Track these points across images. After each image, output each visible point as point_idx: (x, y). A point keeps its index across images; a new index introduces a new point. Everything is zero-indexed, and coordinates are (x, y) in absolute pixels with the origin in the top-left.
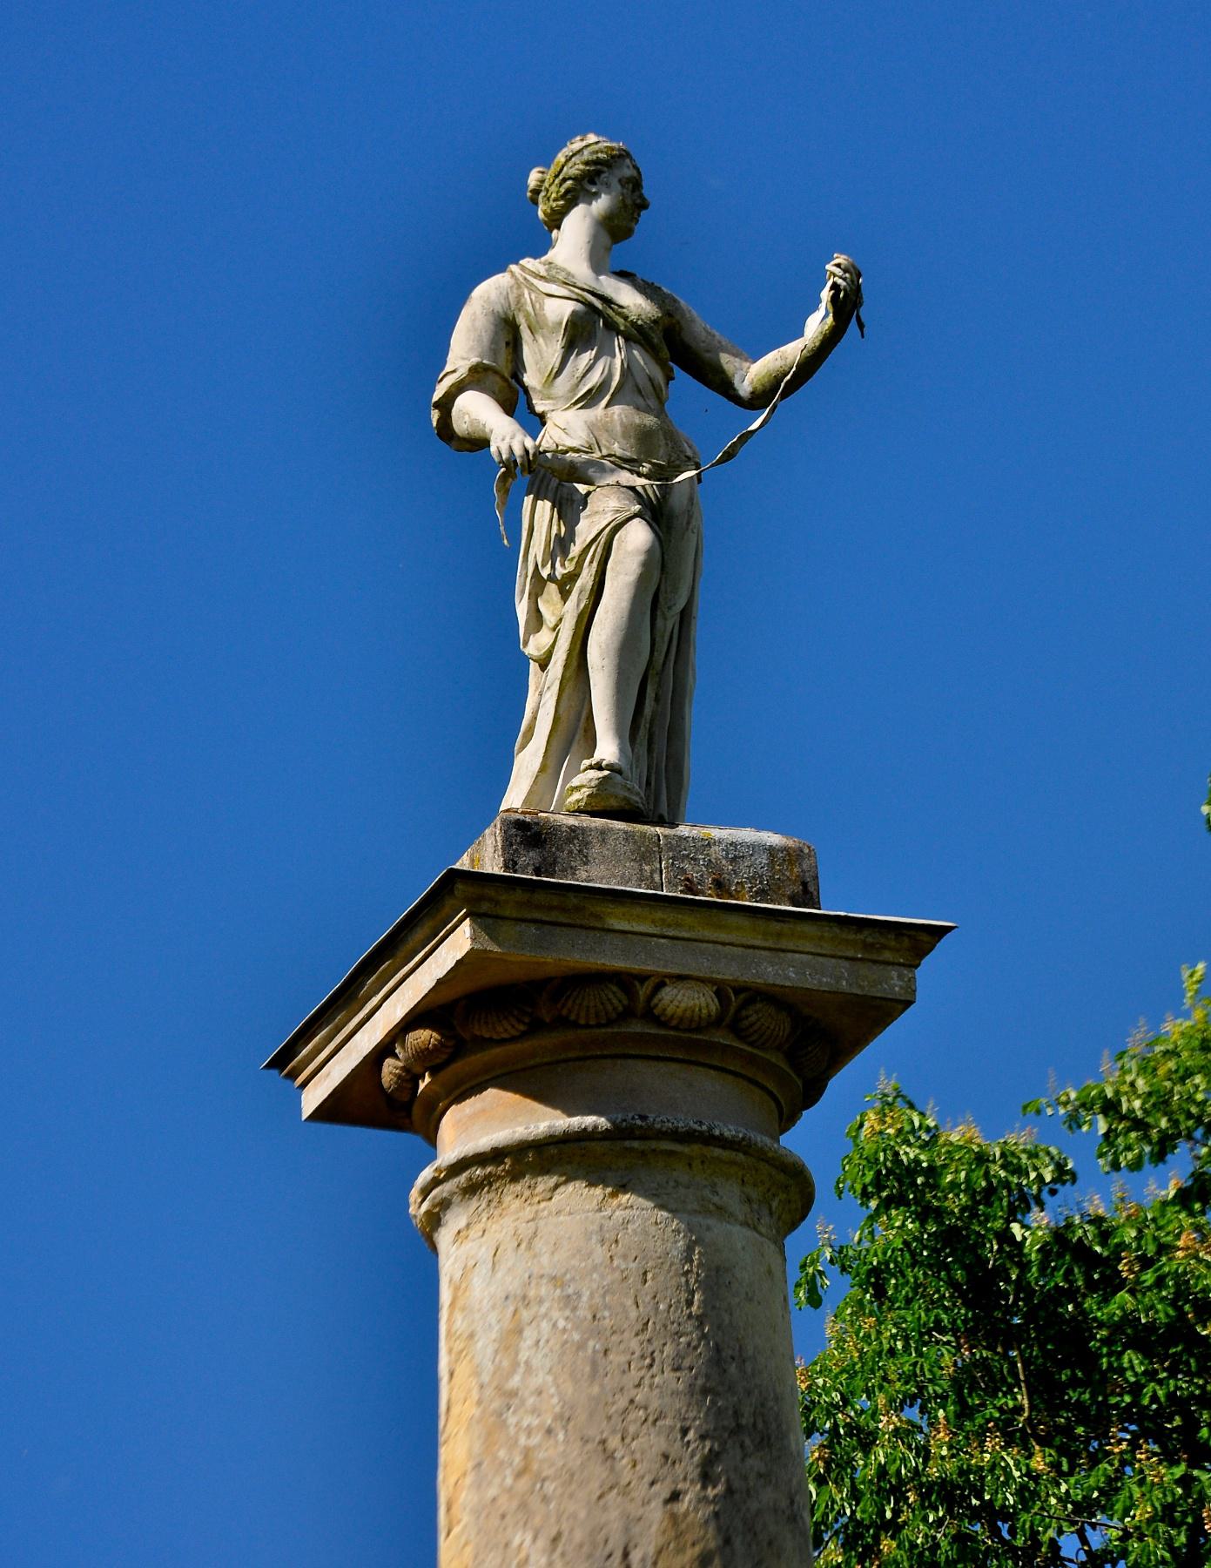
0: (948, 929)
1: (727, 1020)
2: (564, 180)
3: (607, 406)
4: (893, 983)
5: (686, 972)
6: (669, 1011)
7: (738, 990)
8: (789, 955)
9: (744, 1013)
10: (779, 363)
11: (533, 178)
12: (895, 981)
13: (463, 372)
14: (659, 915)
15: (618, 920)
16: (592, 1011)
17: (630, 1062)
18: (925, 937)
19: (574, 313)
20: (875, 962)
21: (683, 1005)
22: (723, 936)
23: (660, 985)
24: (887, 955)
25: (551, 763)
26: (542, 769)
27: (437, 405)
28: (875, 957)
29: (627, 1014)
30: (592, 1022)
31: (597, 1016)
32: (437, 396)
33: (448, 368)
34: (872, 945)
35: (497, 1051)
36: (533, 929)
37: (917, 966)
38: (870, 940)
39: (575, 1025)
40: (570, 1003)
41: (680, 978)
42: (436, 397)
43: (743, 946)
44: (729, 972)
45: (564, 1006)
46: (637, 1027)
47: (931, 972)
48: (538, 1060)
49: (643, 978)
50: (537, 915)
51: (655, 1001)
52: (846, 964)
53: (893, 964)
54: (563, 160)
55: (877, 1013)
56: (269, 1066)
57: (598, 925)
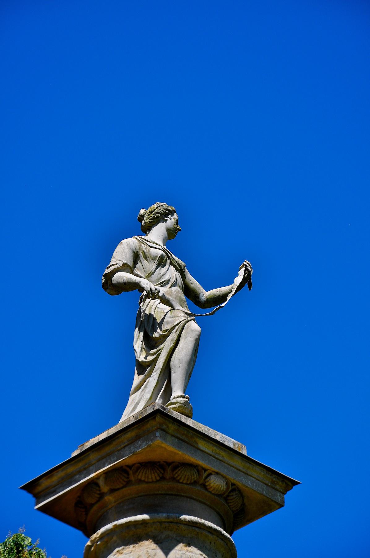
0: (298, 483)
1: (225, 495)
2: (157, 213)
3: (170, 287)
4: (278, 497)
5: (220, 472)
6: (209, 485)
7: (233, 484)
8: (251, 478)
9: (232, 494)
10: (218, 293)
11: (142, 211)
12: (279, 497)
13: (120, 264)
14: (215, 448)
15: (202, 445)
16: (187, 477)
17: (192, 501)
18: (290, 483)
19: (162, 255)
20: (273, 488)
21: (217, 484)
22: (231, 463)
23: (210, 474)
24: (277, 487)
25: (153, 397)
26: (151, 398)
27: (105, 276)
28: (274, 486)
29: (195, 483)
30: (184, 482)
31: (188, 480)
32: (108, 271)
33: (111, 263)
34: (274, 481)
35: (144, 486)
36: (176, 440)
37: (285, 494)
38: (274, 479)
39: (178, 481)
40: (179, 472)
41: (217, 473)
42: (106, 272)
43: (236, 468)
44: (232, 477)
45: (176, 473)
46: (198, 488)
47: (289, 496)
48: (160, 492)
49: (205, 470)
50: (179, 435)
51: (208, 479)
52: (265, 486)
53: (278, 491)
54: (156, 207)
55: (268, 506)
56: (23, 488)
57: (196, 446)
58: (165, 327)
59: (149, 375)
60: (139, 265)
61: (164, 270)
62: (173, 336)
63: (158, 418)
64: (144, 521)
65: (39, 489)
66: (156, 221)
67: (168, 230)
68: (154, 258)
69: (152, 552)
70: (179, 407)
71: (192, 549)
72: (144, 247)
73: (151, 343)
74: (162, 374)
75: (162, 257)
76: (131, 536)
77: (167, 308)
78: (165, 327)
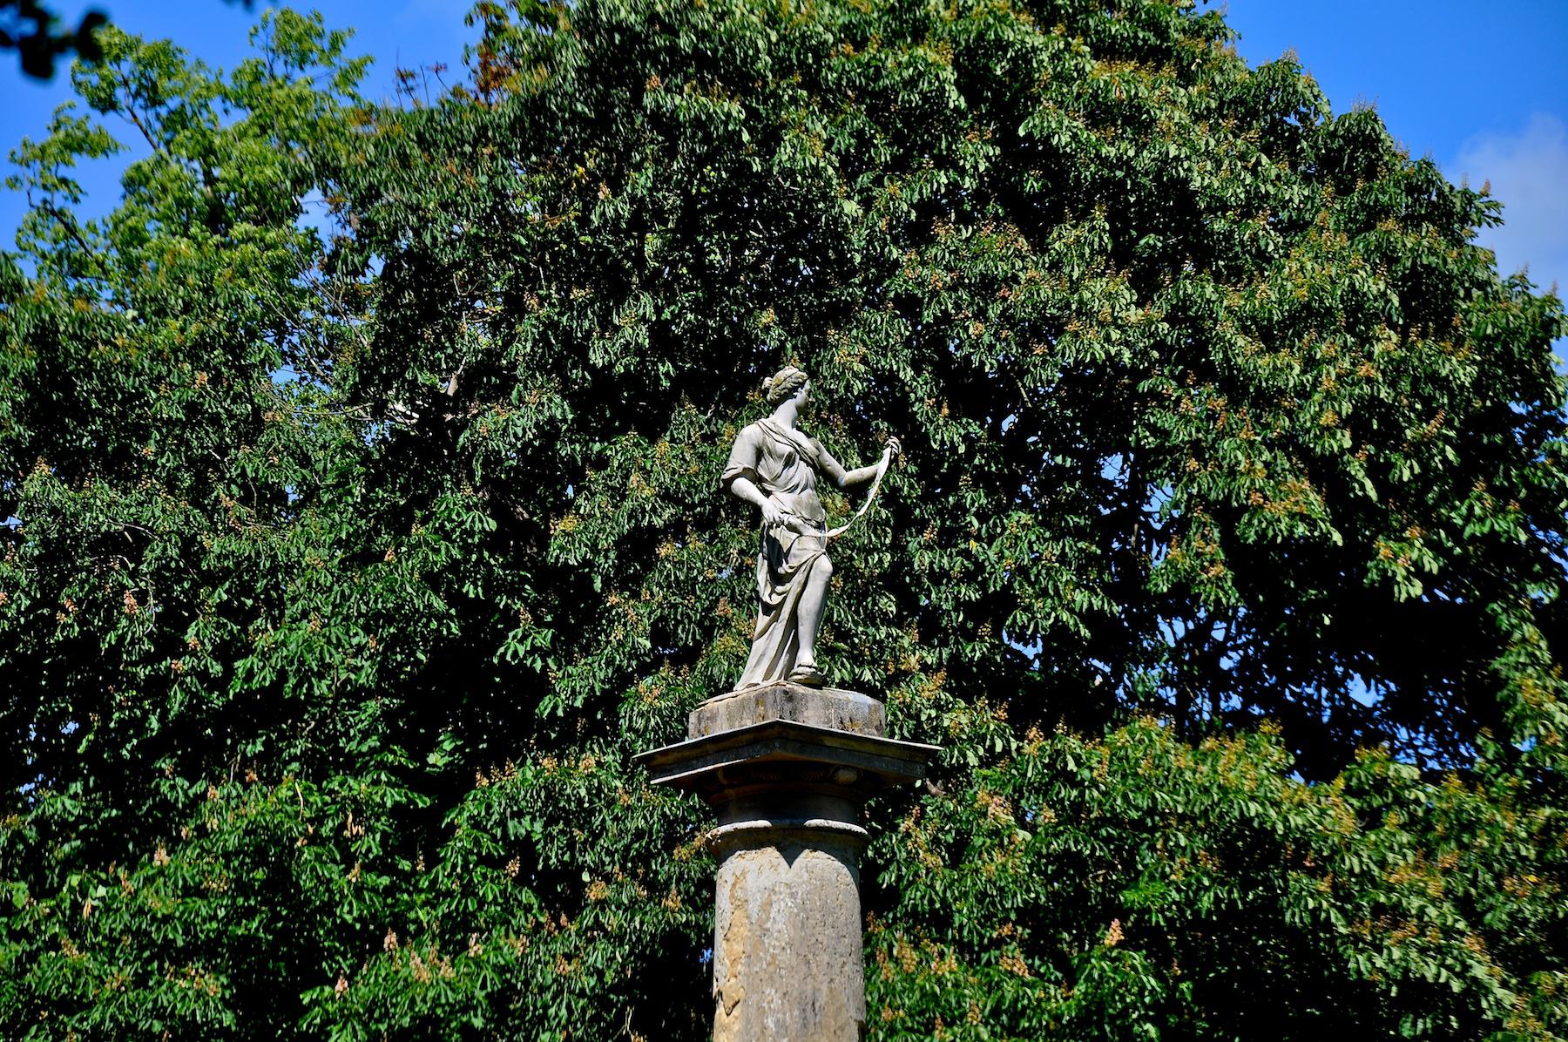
44: (863, 765)
58: (794, 562)
59: (776, 619)
60: (763, 462)
61: (793, 469)
62: (799, 578)
63: (777, 728)
64: (765, 828)
65: (655, 763)
66: (783, 398)
67: (799, 408)
68: (780, 457)
69: (776, 862)
70: (755, 381)
71: (820, 854)
72: (769, 440)
73: (777, 579)
74: (747, 737)
75: (790, 455)
76: (753, 841)
77: (795, 535)
78: (794, 562)
